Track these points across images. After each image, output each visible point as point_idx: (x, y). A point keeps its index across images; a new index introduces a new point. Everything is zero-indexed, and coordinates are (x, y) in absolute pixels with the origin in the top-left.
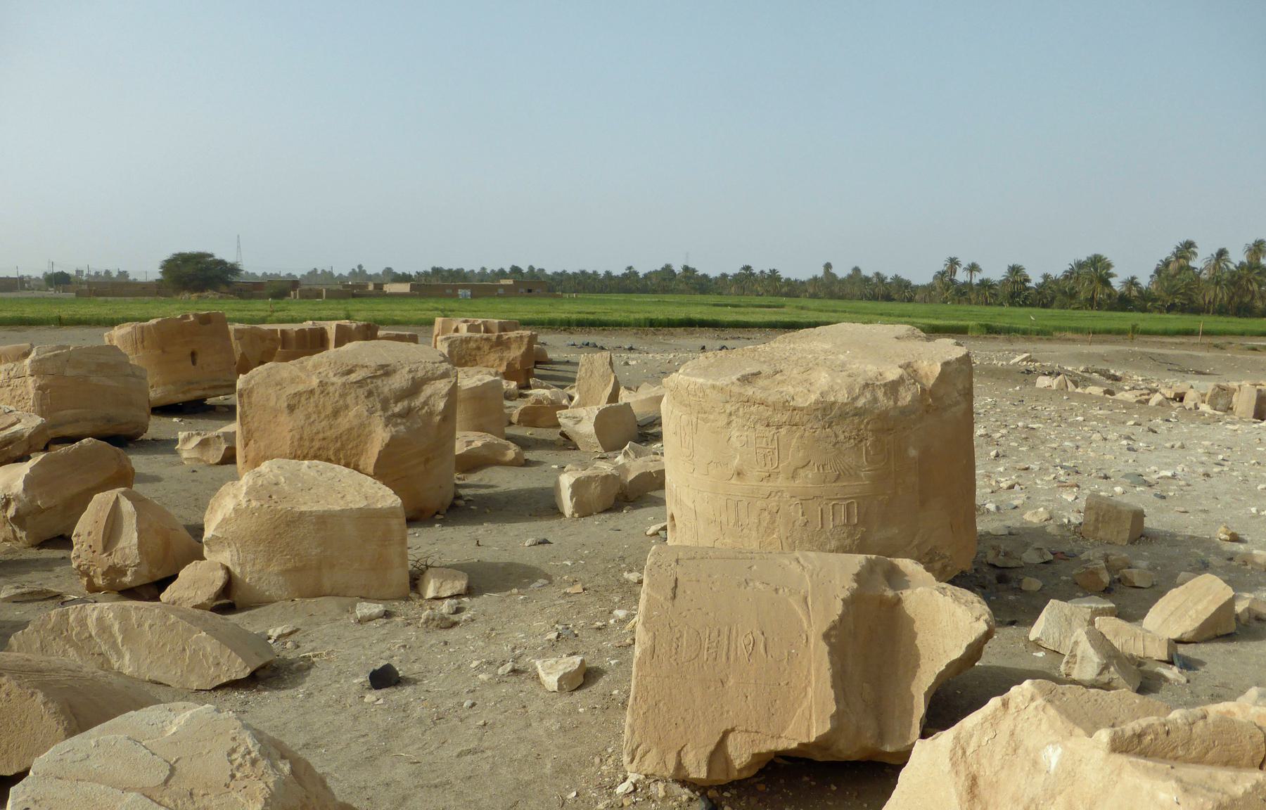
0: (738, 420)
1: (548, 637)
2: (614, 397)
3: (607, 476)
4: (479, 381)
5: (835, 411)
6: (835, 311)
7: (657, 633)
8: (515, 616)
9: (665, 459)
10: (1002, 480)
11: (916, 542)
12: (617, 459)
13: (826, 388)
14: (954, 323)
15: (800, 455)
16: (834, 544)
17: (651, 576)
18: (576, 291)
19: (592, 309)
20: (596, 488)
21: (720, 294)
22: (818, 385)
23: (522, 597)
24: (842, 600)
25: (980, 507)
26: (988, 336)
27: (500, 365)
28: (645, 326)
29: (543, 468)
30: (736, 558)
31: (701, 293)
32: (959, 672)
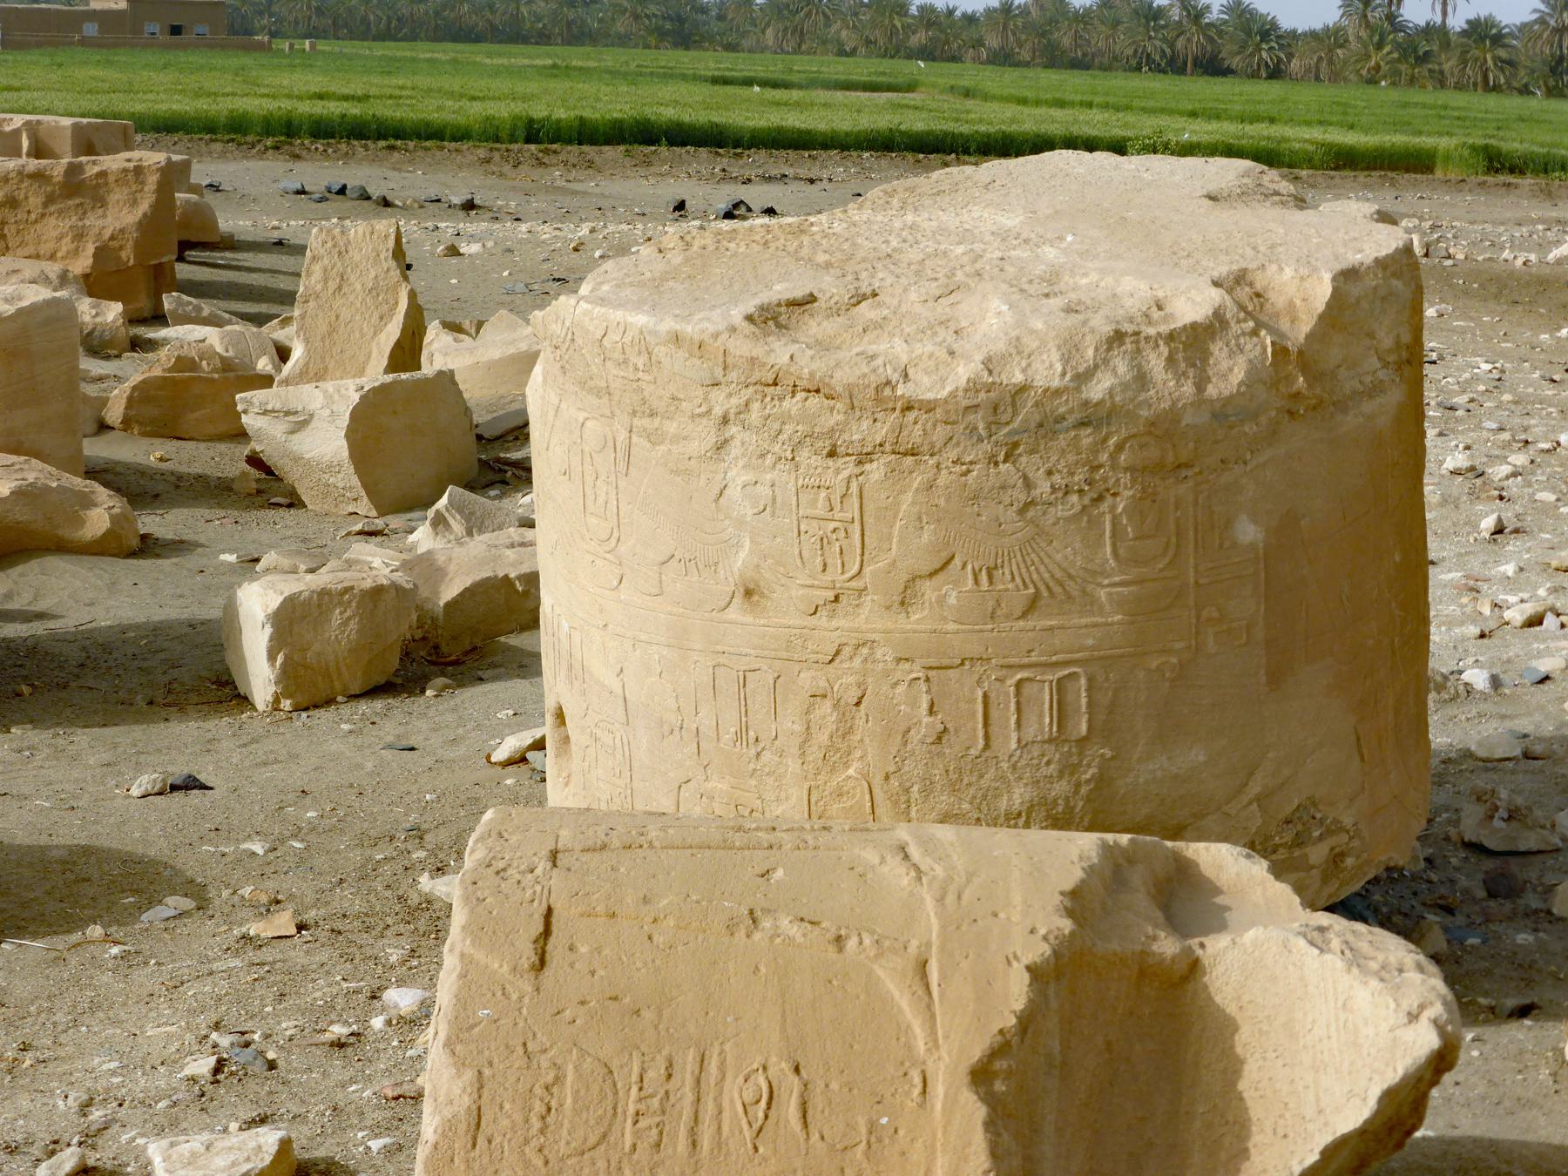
0: (746, 436)
1: (188, 1071)
2: (407, 353)
3: (378, 591)
4: (6, 300)
5: (1026, 409)
6: (1060, 104)
7: (487, 1072)
8: (94, 1007)
9: (542, 550)
10: (1512, 599)
11: (1255, 788)
12: (412, 538)
13: (1000, 346)
14: (1399, 140)
15: (926, 537)
16: (1019, 796)
17: (474, 900)
18: (313, 34)
19: (356, 87)
20: (345, 623)
21: (731, 48)
22: (977, 338)
23: (115, 950)
24: (1028, 968)
25: (1446, 678)
26: (1490, 179)
27: (76, 253)
28: (513, 140)
29: (193, 561)
30: (727, 846)
31: (676, 45)
32: (1362, 1163)
